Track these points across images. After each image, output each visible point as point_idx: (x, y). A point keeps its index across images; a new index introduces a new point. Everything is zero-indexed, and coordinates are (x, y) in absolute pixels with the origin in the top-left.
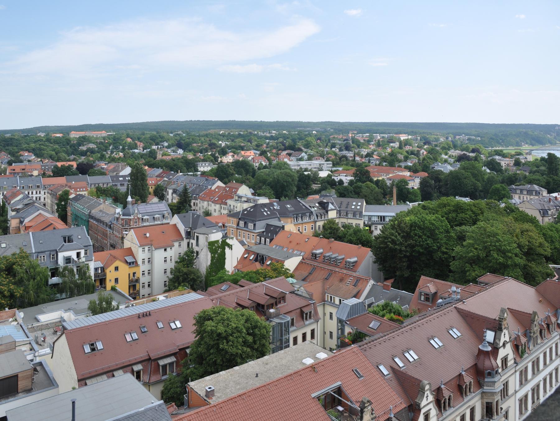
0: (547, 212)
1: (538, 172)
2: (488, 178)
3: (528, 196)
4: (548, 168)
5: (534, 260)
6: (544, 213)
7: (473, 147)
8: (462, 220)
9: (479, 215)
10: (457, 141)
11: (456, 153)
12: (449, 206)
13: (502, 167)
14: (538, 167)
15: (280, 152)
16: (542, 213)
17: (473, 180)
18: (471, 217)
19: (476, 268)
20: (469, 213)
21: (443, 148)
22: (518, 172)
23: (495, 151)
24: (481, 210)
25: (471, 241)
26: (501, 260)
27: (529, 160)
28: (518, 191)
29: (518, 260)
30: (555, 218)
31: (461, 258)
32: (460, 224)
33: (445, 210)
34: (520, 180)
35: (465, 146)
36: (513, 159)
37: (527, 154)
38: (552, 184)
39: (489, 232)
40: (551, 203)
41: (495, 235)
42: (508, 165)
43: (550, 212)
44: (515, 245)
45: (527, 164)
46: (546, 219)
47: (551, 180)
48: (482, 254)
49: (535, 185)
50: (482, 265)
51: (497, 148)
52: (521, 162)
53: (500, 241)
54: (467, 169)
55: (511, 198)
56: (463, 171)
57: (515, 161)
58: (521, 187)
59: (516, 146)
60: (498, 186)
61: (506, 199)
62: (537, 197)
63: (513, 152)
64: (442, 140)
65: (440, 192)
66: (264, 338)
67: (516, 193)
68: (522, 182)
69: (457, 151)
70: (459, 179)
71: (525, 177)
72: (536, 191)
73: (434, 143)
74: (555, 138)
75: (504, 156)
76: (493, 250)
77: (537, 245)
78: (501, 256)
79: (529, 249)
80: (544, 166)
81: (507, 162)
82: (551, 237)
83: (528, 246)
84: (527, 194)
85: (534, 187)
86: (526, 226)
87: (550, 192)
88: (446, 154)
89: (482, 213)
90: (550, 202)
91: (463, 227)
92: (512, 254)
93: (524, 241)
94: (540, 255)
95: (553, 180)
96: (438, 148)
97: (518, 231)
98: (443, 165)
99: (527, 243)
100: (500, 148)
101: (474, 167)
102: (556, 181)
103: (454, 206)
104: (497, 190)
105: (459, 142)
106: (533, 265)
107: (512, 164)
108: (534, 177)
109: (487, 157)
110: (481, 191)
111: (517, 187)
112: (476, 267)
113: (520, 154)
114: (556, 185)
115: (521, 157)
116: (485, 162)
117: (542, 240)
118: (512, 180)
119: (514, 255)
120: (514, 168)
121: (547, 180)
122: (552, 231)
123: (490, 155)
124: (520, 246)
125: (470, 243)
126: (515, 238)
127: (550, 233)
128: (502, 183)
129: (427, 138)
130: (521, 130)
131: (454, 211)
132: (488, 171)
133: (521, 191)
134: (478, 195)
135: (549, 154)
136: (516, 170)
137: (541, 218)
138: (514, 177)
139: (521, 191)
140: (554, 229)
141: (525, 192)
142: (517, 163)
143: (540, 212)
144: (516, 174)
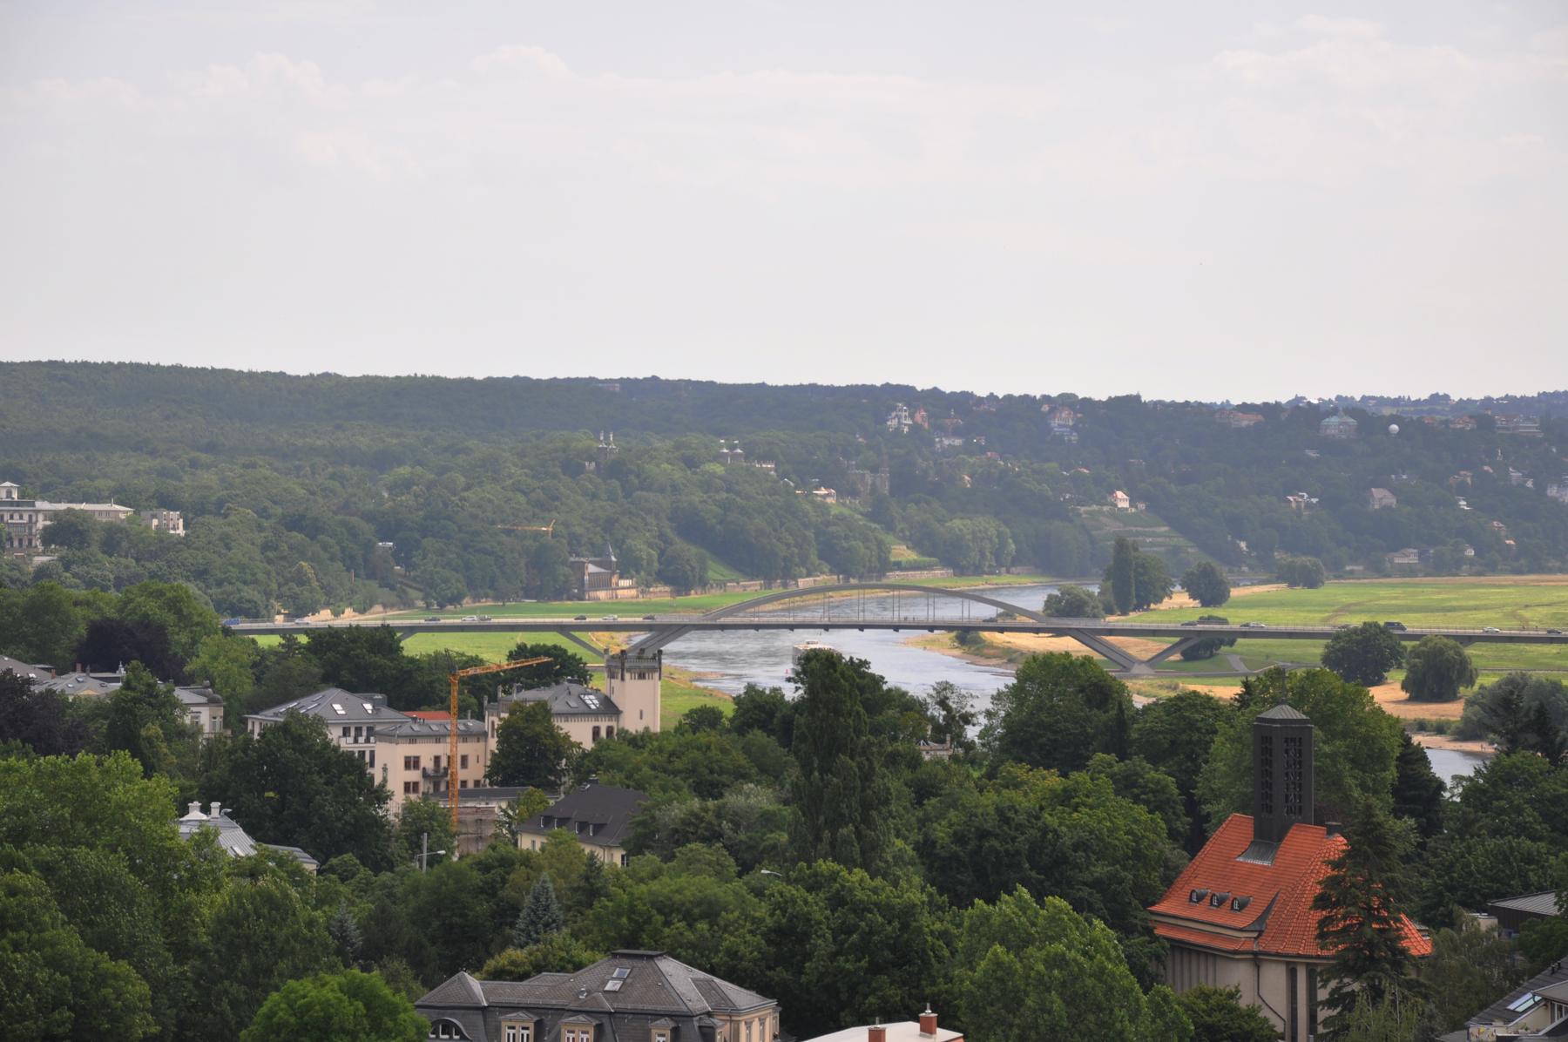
1: (711, 837)
2: (230, 922)
13: (381, 796)
14: (708, 788)
15: (1532, 738)
17: (69, 940)
22: (526, 842)
23: (325, 640)
27: (632, 723)
34: (542, 922)
36: (493, 720)
37: (619, 665)
38: (822, 944)
42: (438, 776)
45: (622, 755)
47: (815, 905)
51: (349, 618)
52: (561, 745)
58: (541, 988)
60: (323, 989)
63: (494, 653)
68: (559, 937)
71: (590, 887)
75: (410, 688)
80: (768, 772)
81: (426, 752)
95: (838, 901)
100: (372, 619)
101: (90, 815)
102: (861, 909)
107: (474, 772)
108: (663, 887)
109: (234, 718)
111: (509, 991)
113: (553, 667)
115: (555, 696)
116: (212, 752)
120: (498, 806)
121: (781, 906)
123: (278, 678)
128: (370, 955)
130: (582, 440)
132: (237, 843)
135: (821, 670)
136: (517, 825)
138: (489, 890)
142: (528, 759)
144: (506, 863)
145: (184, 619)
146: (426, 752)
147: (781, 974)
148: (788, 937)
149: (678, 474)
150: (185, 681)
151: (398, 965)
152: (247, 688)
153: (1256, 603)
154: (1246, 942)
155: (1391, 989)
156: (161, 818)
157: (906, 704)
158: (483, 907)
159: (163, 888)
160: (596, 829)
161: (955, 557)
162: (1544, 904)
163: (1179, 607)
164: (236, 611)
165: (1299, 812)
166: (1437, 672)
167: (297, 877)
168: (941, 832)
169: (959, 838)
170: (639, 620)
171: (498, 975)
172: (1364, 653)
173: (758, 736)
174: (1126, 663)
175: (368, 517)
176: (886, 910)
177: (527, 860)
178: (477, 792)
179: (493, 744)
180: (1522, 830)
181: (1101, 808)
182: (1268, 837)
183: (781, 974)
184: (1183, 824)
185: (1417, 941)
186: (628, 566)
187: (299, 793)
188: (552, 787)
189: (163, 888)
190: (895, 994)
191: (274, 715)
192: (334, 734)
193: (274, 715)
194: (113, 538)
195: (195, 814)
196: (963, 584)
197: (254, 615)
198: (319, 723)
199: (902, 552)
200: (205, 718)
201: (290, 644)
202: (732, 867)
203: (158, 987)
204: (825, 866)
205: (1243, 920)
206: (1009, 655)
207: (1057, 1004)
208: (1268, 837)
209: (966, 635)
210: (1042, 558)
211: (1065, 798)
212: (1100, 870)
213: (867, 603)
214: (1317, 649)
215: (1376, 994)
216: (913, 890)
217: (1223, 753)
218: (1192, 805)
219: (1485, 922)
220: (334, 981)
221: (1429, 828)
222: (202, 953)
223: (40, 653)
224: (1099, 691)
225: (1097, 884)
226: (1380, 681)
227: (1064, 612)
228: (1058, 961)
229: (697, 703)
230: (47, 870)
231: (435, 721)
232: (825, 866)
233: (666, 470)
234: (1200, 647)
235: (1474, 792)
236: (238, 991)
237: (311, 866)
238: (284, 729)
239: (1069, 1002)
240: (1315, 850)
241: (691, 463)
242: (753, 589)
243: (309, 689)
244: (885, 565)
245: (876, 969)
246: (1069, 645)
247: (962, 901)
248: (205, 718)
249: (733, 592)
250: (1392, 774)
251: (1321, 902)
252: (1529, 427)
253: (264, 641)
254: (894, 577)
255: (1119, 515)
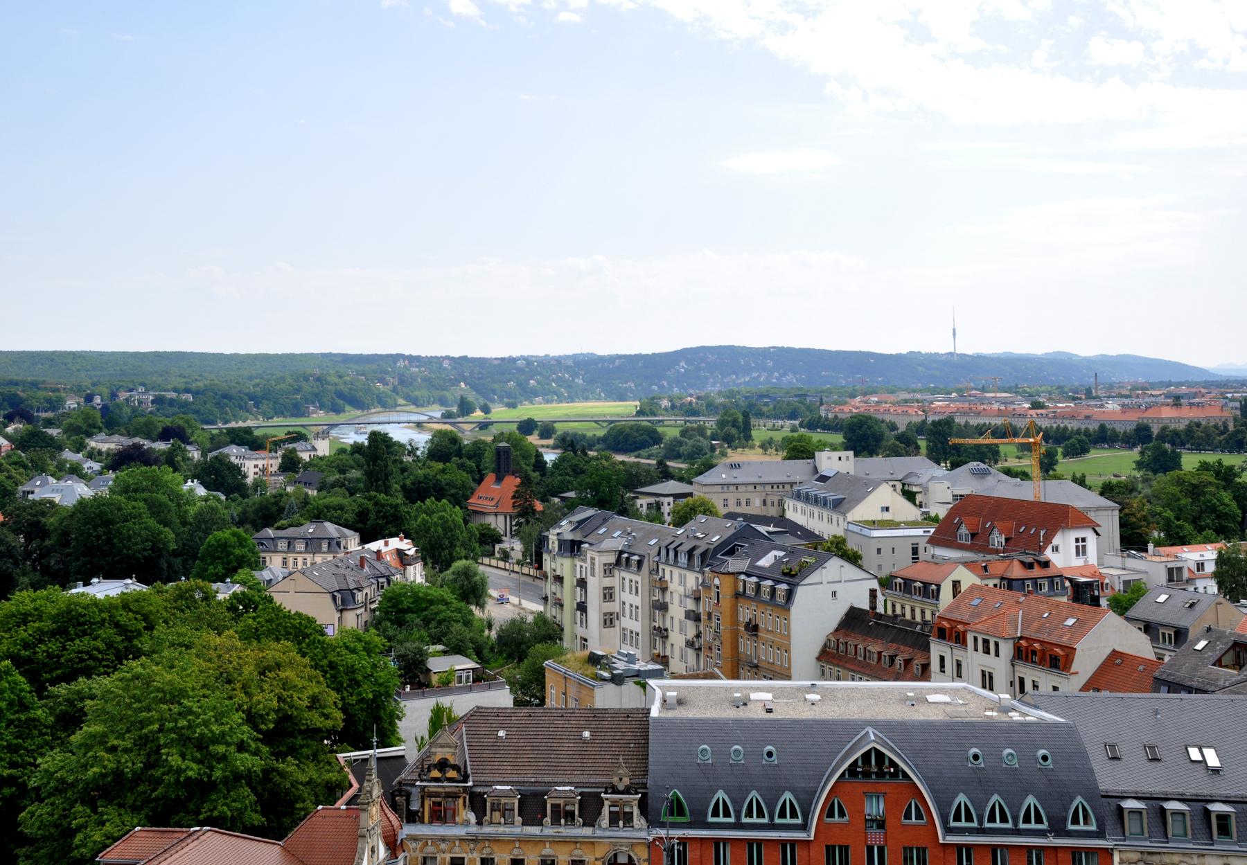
0: (353, 596)
1: (342, 485)
3: (309, 557)
4: (366, 473)
5: (293, 751)
6: (344, 599)
7: (168, 422)
8: (82, 660)
9: (139, 634)
10: (119, 406)
11: (106, 444)
12: (40, 618)
14: (342, 471)
16: (339, 602)
17: (152, 522)
18: (110, 645)
19: (110, 812)
20: (108, 632)
21: (72, 430)
23: (231, 431)
24: (146, 618)
25: (97, 728)
26: (193, 770)
27: (320, 453)
28: (282, 545)
29: (246, 762)
30: (374, 611)
31: (62, 787)
32: (70, 678)
33: (23, 633)
35: (142, 420)
36: (280, 453)
37: (317, 436)
38: (372, 516)
39: (158, 690)
40: (366, 569)
41: (176, 696)
42: (264, 470)
43: (360, 597)
44: (238, 717)
45: (317, 463)
46: (352, 620)
47: (370, 505)
48: (132, 764)
49: (328, 525)
50: (130, 799)
51: (241, 424)
52: (299, 460)
53: (190, 712)
54: (136, 491)
55: (259, 565)
56: (122, 499)
57: (284, 457)
58: (290, 532)
59: (293, 415)
60: (225, 534)
61: (247, 570)
62: (330, 557)
64: (71, 403)
65: (46, 571)
66: (353, 672)
67: (276, 551)
68: (296, 516)
69: (116, 438)
70: (108, 523)
71: (306, 501)
72: (330, 540)
73: (44, 415)
74: (395, 390)
75: (254, 444)
76: (166, 746)
77: (306, 703)
78: (194, 760)
79: (278, 722)
80: (360, 466)
81: (260, 463)
82: (351, 670)
83: (277, 712)
84: (306, 551)
85: (325, 530)
86: (275, 650)
87: (365, 540)
88: (79, 448)
89: (150, 628)
90: (362, 566)
91: (82, 683)
92: (228, 744)
93: (266, 700)
94: (314, 733)
95: (376, 504)
96: (53, 432)
97: (249, 670)
98: (62, 484)
99: (275, 704)
101: (156, 483)
102: (383, 506)
103: (55, 618)
104: (224, 546)
105: (127, 411)
106: (289, 766)
107: (275, 469)
109: (204, 455)
110: (175, 554)
111: (280, 533)
112: (110, 809)
113: (299, 437)
114: (384, 517)
115: (298, 446)
116: (196, 466)
117: (318, 687)
118: (269, 514)
119: (233, 749)
120: (281, 478)
122: (353, 651)
124: (252, 718)
125: (93, 736)
126: (241, 697)
127: (350, 658)
128: (240, 524)
129: (22, 400)
131: (53, 634)
132: (201, 491)
133: (291, 542)
134: (165, 566)
135: (374, 436)
137: (338, 615)
138: (276, 503)
139: (291, 542)
140: (359, 646)
141: (300, 546)
142: (290, 464)
143: (334, 598)
145: (190, 426)
146: (260, 463)
147: (360, 525)
148: (362, 515)
149: (337, 380)
150: (189, 444)
151: (248, 526)
152: (208, 445)
153: (500, 412)
154: (493, 509)
155: (532, 521)
156: (178, 484)
157: (401, 446)
158: (275, 508)
159: (179, 505)
160: (309, 484)
161: (416, 402)
162: (572, 494)
163: (478, 415)
164: (208, 423)
165: (507, 472)
166: (547, 431)
167: (219, 500)
168: (408, 482)
169: (413, 484)
170: (876, 533)
171: (278, 528)
172: (527, 426)
173: (357, 455)
174: (463, 431)
175: (246, 394)
176: (391, 506)
177: (287, 494)
178: (275, 474)
179: (280, 460)
180: (567, 474)
181: (454, 474)
182: (499, 479)
183: (360, 525)
184: (477, 476)
185: (539, 506)
186: (322, 407)
187: (220, 476)
188: (297, 472)
189: (179, 505)
190: (393, 530)
191: (214, 453)
192: (233, 459)
193: (214, 453)
194: (172, 402)
195: (189, 483)
196: (419, 410)
197: (212, 423)
198: (228, 456)
199: (401, 401)
200: (195, 454)
201: (221, 433)
202: (347, 494)
203: (177, 535)
204: (373, 493)
205: (493, 503)
206: (431, 430)
207: (440, 529)
208: (499, 479)
209: (419, 425)
210: (442, 402)
211: (443, 471)
212: (453, 491)
213: (393, 417)
214: (514, 427)
215: (528, 522)
216: (399, 499)
217: (488, 457)
218: (480, 471)
219: (556, 500)
220: (228, 532)
221: (543, 475)
222: (190, 524)
223: (148, 436)
224: (454, 440)
225: (452, 495)
226: (530, 434)
227: (447, 416)
228: (442, 518)
229: (340, 446)
230: (145, 500)
231: (262, 454)
232: (373, 493)
233: (333, 379)
234: (484, 426)
235: (556, 465)
236: (201, 534)
237: (223, 498)
238: (216, 458)
239: (444, 529)
240: (512, 483)
241: (340, 377)
242: (359, 412)
243: (226, 445)
244: (396, 405)
245: (388, 523)
246: (448, 427)
247: (413, 502)
248: (195, 454)
249: (352, 413)
250: (533, 460)
251: (513, 497)
252: (570, 363)
253: (214, 432)
254: (399, 408)
255: (462, 389)
